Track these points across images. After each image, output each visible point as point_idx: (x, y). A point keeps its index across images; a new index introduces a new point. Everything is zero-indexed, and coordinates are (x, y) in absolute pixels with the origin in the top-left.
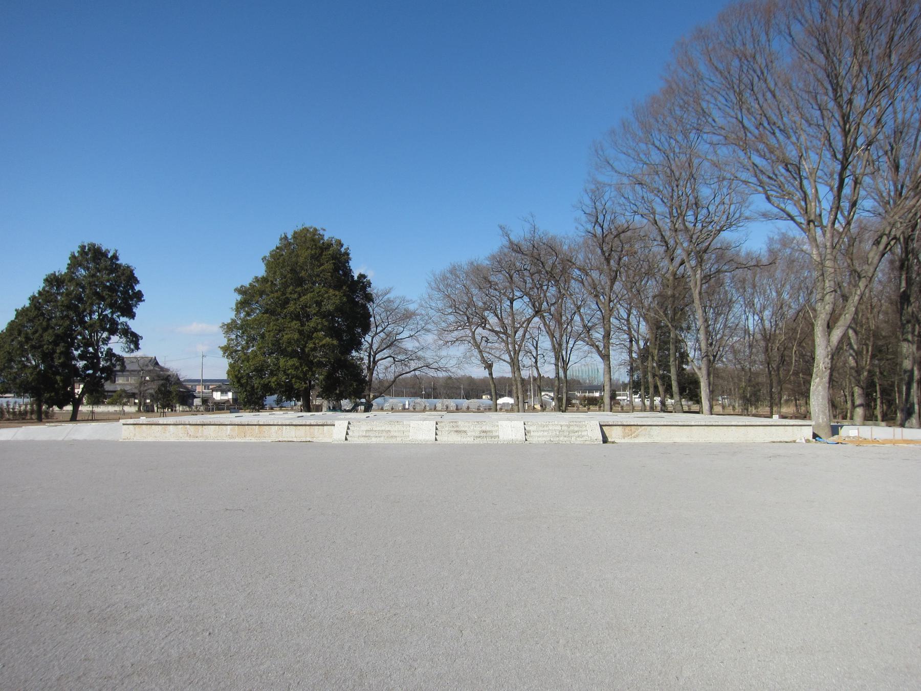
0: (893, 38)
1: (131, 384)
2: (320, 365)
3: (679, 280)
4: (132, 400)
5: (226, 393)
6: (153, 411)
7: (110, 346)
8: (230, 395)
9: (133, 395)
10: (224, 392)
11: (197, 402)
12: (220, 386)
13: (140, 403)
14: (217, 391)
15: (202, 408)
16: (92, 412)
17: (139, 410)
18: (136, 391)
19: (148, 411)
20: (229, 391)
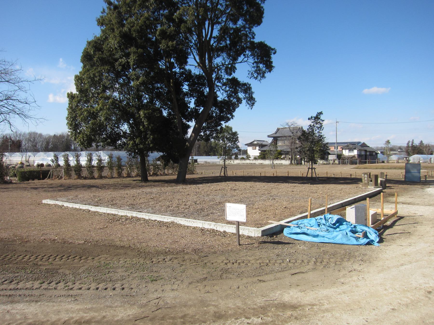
0: (89, 309)
1: (287, 146)
2: (123, 79)
3: (118, 316)
4: (288, 156)
5: (353, 151)
6: (301, 164)
7: (244, 102)
8: (355, 152)
9: (287, 153)
10: (351, 150)
11: (331, 157)
12: (348, 146)
13: (292, 158)
14: (346, 149)
15: (337, 162)
16: (225, 167)
17: (291, 163)
18: (289, 150)
19: (298, 164)
20: (355, 149)
